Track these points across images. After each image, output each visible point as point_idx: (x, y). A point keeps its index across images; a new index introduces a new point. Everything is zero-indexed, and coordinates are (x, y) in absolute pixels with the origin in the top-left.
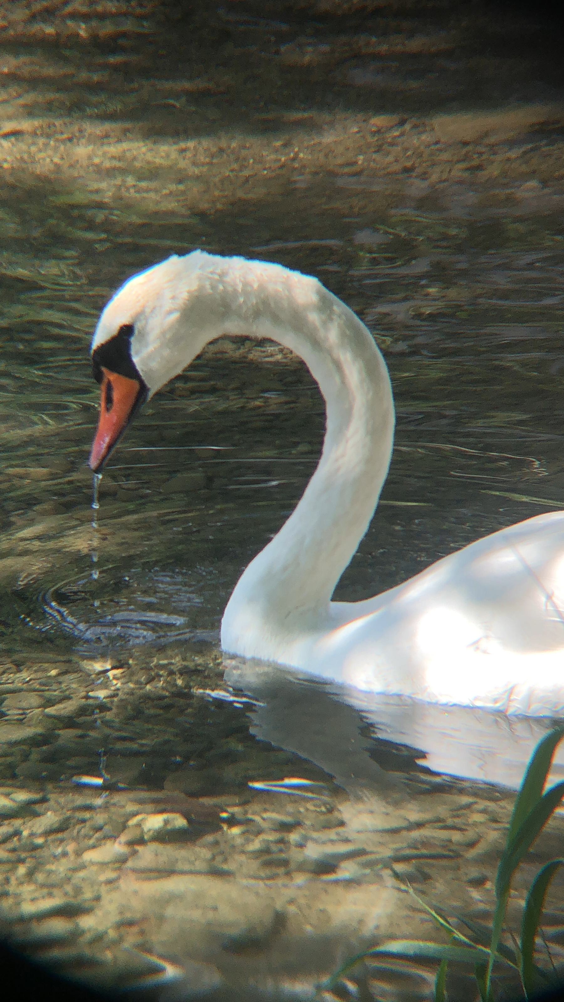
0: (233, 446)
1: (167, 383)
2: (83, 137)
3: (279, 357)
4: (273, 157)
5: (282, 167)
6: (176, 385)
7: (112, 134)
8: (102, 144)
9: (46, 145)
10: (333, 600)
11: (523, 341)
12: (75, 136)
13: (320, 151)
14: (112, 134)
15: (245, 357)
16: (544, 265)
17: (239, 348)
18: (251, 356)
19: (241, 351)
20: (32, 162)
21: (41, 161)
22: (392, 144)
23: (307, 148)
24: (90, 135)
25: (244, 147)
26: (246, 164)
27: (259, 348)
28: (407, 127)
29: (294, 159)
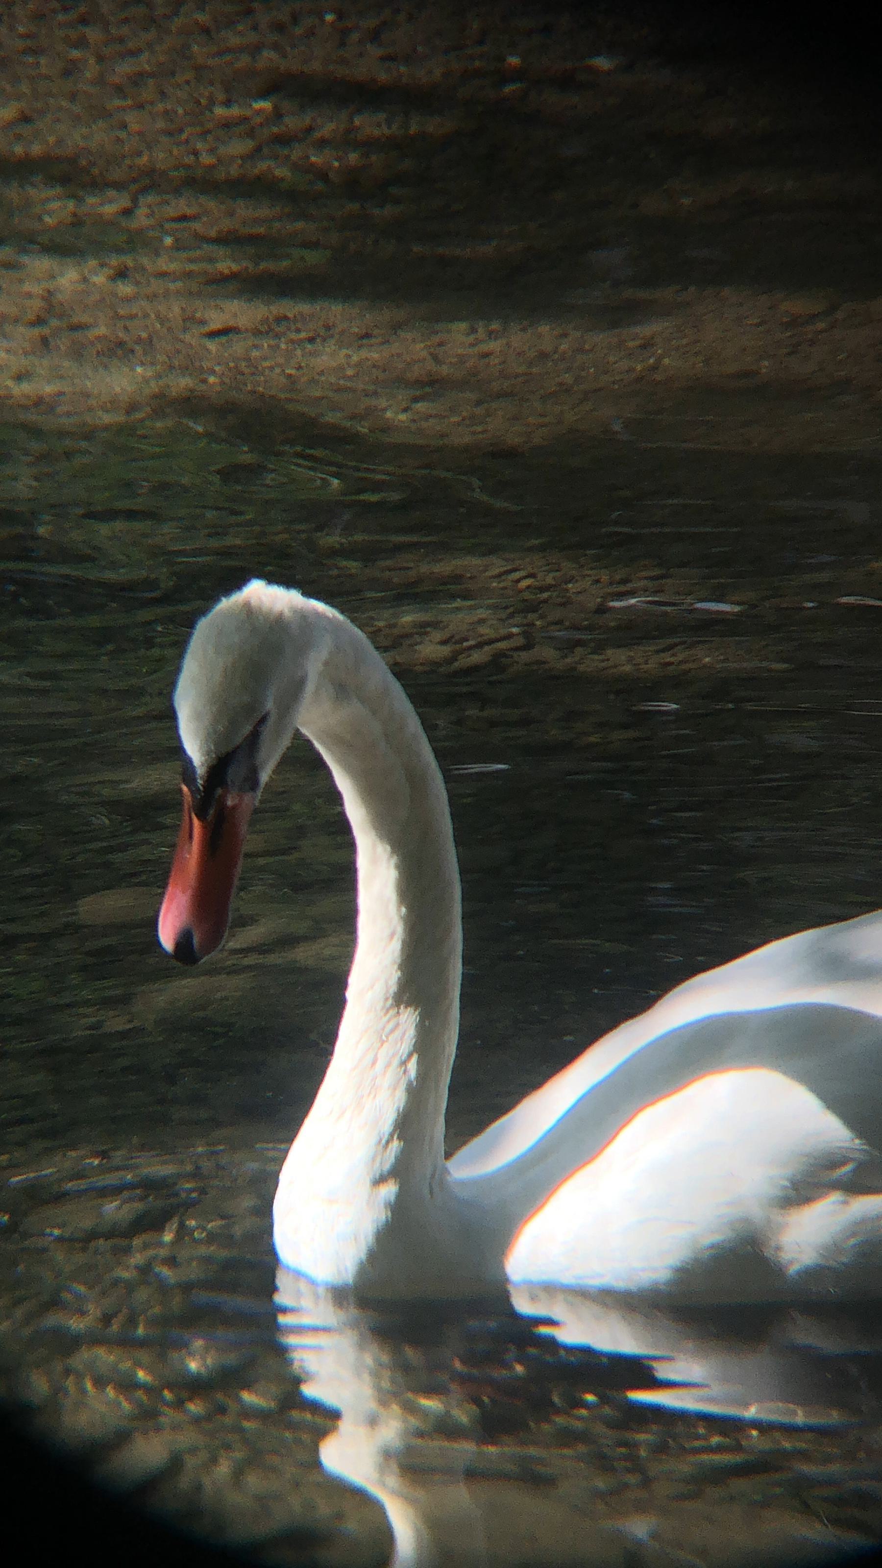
0: (785, 662)
1: (420, 721)
2: (332, 336)
3: (628, 668)
4: (624, 365)
5: (639, 379)
6: (467, 713)
7: (376, 332)
8: (360, 347)
9: (275, 348)
10: (334, 1415)
11: (381, 1163)
12: (319, 335)
13: (696, 354)
14: (376, 332)
15: (575, 669)
16: (88, 1161)
17: (566, 656)
18: (581, 668)
19: (568, 660)
20: (253, 374)
21: (267, 372)
22: (812, 343)
23: (677, 349)
24: (342, 333)
25: (581, 350)
26: (583, 374)
27: (596, 657)
28: (840, 315)
29: (654, 368)
